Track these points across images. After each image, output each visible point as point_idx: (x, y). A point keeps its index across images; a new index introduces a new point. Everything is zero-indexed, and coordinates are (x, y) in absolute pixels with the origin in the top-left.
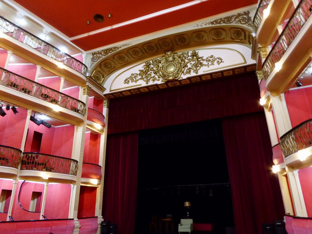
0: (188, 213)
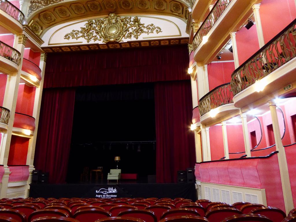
0: (117, 166)
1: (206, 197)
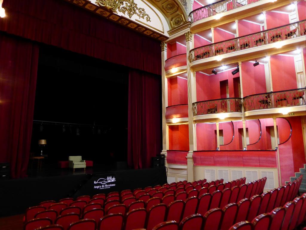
0: (42, 152)
1: (206, 177)
